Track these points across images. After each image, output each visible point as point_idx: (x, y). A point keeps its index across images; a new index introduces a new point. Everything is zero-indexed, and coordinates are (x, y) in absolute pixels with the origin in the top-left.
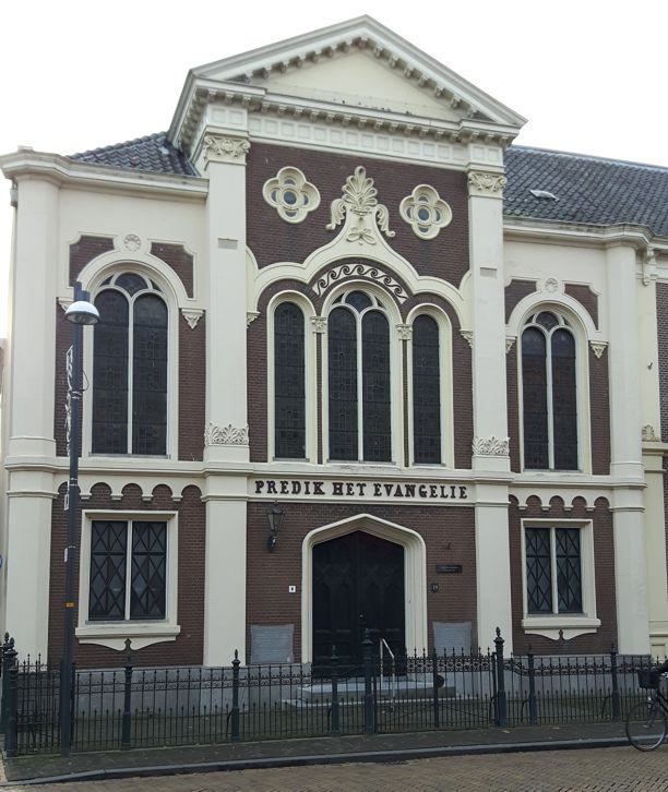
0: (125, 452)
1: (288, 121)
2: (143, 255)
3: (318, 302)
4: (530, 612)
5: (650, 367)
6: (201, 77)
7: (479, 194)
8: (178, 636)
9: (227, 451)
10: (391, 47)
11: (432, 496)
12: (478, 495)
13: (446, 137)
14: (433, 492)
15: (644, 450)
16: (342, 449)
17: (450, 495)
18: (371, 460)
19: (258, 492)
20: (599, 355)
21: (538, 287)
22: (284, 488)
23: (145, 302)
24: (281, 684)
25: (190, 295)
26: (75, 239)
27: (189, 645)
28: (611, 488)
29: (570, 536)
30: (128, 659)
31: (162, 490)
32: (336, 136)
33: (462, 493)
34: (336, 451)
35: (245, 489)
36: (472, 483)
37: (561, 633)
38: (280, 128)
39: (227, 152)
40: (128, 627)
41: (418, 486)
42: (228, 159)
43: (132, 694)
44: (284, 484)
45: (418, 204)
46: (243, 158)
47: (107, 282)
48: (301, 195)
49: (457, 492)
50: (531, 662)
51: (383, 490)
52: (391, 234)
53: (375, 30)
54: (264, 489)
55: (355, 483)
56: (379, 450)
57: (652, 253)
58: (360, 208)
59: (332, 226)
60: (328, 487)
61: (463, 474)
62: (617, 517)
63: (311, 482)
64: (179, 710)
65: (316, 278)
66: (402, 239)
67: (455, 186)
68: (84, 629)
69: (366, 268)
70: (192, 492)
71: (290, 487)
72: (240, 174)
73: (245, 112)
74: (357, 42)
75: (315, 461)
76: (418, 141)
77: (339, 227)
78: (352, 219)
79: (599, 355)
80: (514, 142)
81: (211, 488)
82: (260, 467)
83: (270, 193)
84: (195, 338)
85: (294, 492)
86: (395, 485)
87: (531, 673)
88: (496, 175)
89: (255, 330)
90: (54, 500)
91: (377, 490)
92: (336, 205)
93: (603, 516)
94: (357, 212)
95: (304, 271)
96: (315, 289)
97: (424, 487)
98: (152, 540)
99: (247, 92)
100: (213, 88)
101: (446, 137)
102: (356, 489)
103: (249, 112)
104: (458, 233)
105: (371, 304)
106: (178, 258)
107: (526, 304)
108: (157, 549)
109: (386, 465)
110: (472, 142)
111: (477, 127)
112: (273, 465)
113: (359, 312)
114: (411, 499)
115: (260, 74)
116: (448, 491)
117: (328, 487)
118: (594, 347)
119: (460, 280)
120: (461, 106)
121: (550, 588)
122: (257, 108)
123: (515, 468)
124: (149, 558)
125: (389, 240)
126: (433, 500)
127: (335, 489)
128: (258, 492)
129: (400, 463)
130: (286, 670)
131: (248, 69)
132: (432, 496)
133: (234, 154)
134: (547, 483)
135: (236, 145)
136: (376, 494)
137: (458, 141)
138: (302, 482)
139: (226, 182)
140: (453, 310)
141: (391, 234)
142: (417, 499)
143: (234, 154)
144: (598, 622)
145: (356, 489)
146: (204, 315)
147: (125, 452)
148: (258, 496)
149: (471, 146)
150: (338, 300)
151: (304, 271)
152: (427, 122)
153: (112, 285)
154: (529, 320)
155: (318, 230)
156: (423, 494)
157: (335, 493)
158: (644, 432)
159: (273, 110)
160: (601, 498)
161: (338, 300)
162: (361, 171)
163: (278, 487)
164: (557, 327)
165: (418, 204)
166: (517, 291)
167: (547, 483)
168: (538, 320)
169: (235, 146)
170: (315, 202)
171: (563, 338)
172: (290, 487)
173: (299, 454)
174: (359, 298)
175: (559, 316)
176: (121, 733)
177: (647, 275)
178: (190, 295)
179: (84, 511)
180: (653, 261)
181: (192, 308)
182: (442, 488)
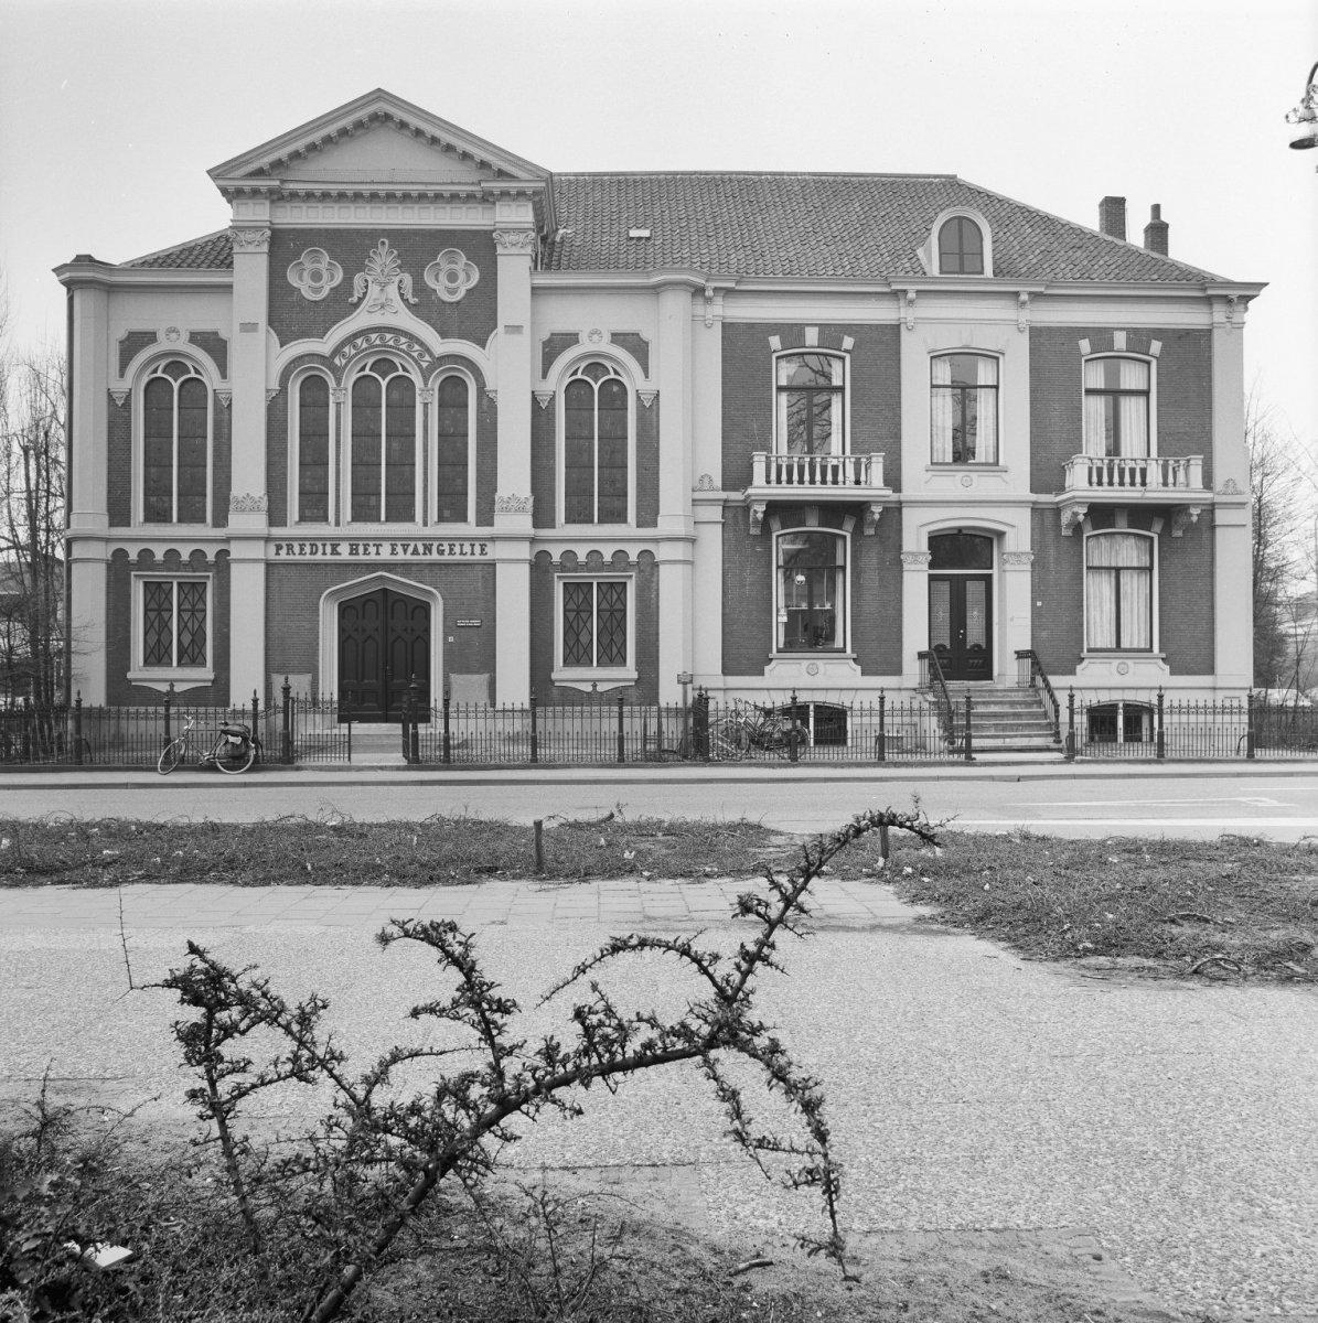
0: (592, 522)
1: (472, 206)
2: (182, 344)
4: (566, 663)
7: (243, 250)
8: (213, 682)
9: (248, 521)
12: (495, 552)
13: (470, 197)
14: (451, 550)
17: (470, 552)
18: (626, 517)
19: (277, 554)
20: (120, 403)
22: (302, 549)
23: (574, 391)
25: (224, 376)
27: (219, 690)
28: (656, 540)
29: (194, 590)
30: (169, 699)
32: (361, 213)
33: (483, 550)
36: (493, 539)
37: (595, 686)
38: (289, 212)
40: (174, 672)
41: (436, 544)
42: (251, 248)
49: (477, 549)
51: (399, 549)
52: (413, 300)
54: (284, 551)
56: (401, 509)
58: (382, 279)
60: (344, 549)
61: (485, 531)
62: (234, 567)
65: (337, 351)
66: (424, 304)
67: (482, 247)
68: (138, 671)
71: (307, 549)
73: (267, 203)
74: (374, 117)
75: (341, 524)
76: (302, 204)
77: (361, 300)
78: (374, 290)
82: (277, 531)
84: (224, 411)
85: (311, 553)
86: (412, 544)
88: (523, 231)
90: (108, 564)
91: (393, 549)
92: (358, 280)
93: (648, 566)
95: (324, 346)
96: (337, 361)
98: (196, 599)
99: (263, 184)
101: (470, 197)
102: (372, 550)
103: (272, 202)
104: (486, 293)
106: (637, 346)
108: (618, 606)
111: (498, 186)
112: (294, 529)
114: (428, 557)
115: (278, 164)
116: (467, 548)
117: (344, 549)
118: (114, 396)
119: (285, 344)
120: (483, 165)
121: (179, 635)
122: (277, 197)
125: (414, 309)
126: (451, 557)
127: (352, 549)
128: (277, 554)
131: (265, 162)
132: (450, 553)
133: (520, 245)
134: (577, 539)
135: (523, 236)
138: (319, 544)
139: (251, 273)
141: (413, 300)
143: (520, 245)
145: (372, 550)
146: (554, 396)
147: (592, 522)
148: (277, 557)
151: (324, 346)
153: (579, 376)
155: (341, 303)
159: (294, 195)
160: (143, 550)
163: (297, 549)
166: (553, 347)
167: (577, 539)
169: (257, 236)
171: (615, 389)
172: (307, 549)
174: (383, 366)
178: (224, 376)
179: (133, 573)
182: (462, 545)
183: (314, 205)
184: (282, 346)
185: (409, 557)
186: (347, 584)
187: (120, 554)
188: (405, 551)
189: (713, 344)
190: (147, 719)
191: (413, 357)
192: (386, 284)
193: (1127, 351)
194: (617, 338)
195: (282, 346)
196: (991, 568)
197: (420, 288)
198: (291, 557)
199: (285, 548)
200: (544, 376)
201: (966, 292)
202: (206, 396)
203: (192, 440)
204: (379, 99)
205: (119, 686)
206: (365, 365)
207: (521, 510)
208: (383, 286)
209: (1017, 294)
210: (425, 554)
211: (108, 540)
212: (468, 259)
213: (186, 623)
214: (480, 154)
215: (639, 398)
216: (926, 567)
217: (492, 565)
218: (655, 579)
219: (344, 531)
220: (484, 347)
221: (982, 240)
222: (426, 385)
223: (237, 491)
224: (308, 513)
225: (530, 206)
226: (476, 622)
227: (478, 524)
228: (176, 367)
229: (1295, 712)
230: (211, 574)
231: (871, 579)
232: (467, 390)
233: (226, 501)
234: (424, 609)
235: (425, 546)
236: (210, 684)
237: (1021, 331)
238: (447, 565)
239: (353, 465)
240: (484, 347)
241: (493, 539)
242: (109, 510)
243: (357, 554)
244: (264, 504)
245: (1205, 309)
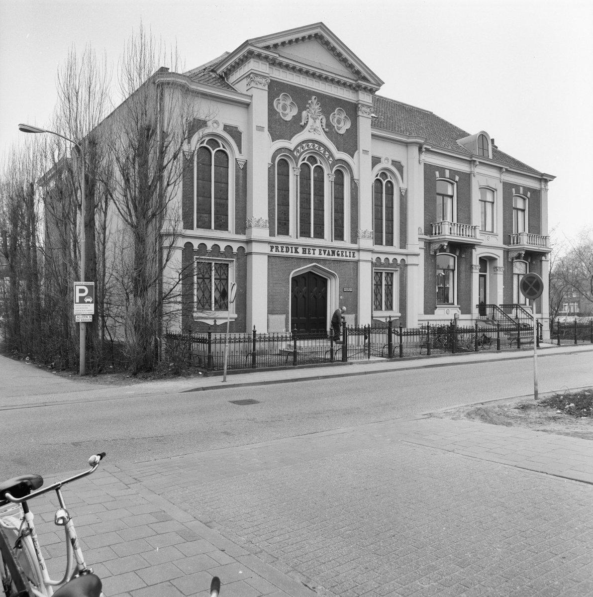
2: (220, 131)
6: (252, 45)
9: (260, 232)
13: (350, 86)
14: (342, 254)
16: (305, 233)
17: (345, 255)
18: (227, 226)
19: (271, 251)
20: (242, 167)
22: (282, 249)
24: (235, 343)
25: (240, 152)
27: (242, 323)
28: (407, 255)
29: (223, 268)
33: (354, 255)
34: (302, 232)
35: (266, 249)
36: (359, 250)
37: (215, 321)
42: (260, 86)
43: (212, 345)
44: (282, 248)
45: (282, 102)
46: (267, 87)
48: (289, 107)
50: (401, 331)
51: (322, 252)
52: (327, 130)
53: (324, 31)
54: (274, 250)
55: (311, 248)
58: (314, 116)
59: (302, 123)
60: (300, 250)
63: (294, 247)
64: (221, 353)
65: (295, 148)
66: (330, 132)
67: (352, 110)
69: (316, 145)
71: (285, 249)
75: (293, 237)
76: (259, 61)
77: (306, 124)
78: (311, 121)
80: (377, 93)
83: (278, 107)
84: (243, 172)
87: (401, 335)
89: (271, 170)
91: (320, 252)
92: (304, 113)
93: (404, 265)
95: (292, 144)
96: (295, 153)
100: (257, 51)
101: (350, 86)
102: (312, 252)
103: (269, 64)
104: (353, 132)
105: (219, 147)
106: (400, 167)
107: (378, 167)
110: (253, 58)
113: (312, 165)
114: (333, 257)
116: (348, 254)
117: (300, 250)
118: (185, 153)
120: (358, 73)
122: (274, 63)
123: (272, 234)
124: (204, 280)
125: (326, 132)
128: (271, 251)
129: (231, 233)
130: (284, 336)
131: (271, 43)
135: (369, 109)
138: (279, 246)
141: (327, 130)
142: (336, 257)
143: (263, 85)
144: (400, 315)
145: (312, 252)
149: (360, 92)
150: (304, 160)
151: (292, 144)
153: (205, 145)
154: (377, 176)
155: (297, 125)
156: (338, 255)
159: (280, 65)
162: (315, 98)
163: (280, 249)
164: (387, 180)
165: (282, 102)
168: (380, 176)
169: (263, 81)
170: (295, 112)
171: (389, 185)
173: (287, 233)
176: (256, 359)
178: (240, 152)
182: (346, 252)
183: (257, 61)
185: (326, 256)
186: (324, 268)
187: (189, 245)
190: (220, 342)
193: (440, 177)
194: (226, 128)
196: (486, 272)
197: (329, 125)
198: (277, 253)
201: (516, 172)
203: (220, 184)
205: (189, 325)
208: (315, 119)
209: (501, 168)
211: (372, 252)
214: (358, 67)
216: (478, 271)
217: (357, 262)
218: (405, 272)
219: (295, 241)
220: (273, 141)
221: (488, 145)
226: (350, 290)
229: (365, 331)
230: (234, 259)
231: (463, 275)
232: (343, 177)
236: (234, 320)
238: (340, 261)
240: (273, 141)
241: (359, 250)
245: (468, 165)
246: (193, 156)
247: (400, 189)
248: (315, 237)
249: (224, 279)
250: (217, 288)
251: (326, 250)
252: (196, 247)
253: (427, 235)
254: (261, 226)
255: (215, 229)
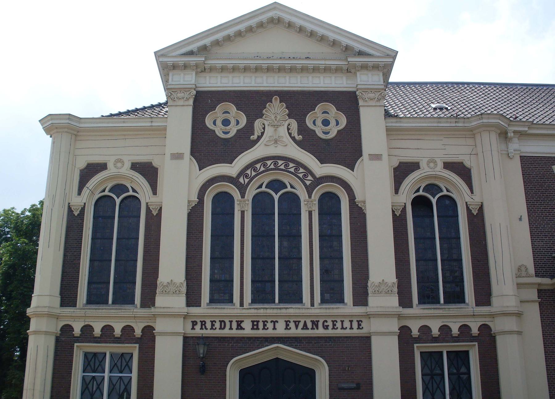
2: (440, 170)
3: (243, 189)
5: (520, 219)
7: (366, 104)
10: (294, 19)
11: (333, 328)
12: (369, 327)
14: (334, 325)
15: (518, 284)
17: (349, 327)
19: (193, 328)
20: (76, 213)
21: (130, 166)
22: (213, 325)
25: (155, 193)
26: (155, 164)
31: (464, 329)
33: (359, 325)
36: (368, 316)
39: (371, 99)
42: (181, 102)
47: (418, 190)
51: (292, 325)
54: (198, 327)
57: (512, 134)
59: (254, 137)
60: (247, 325)
61: (360, 310)
62: (158, 340)
65: (242, 173)
70: (484, 328)
72: (188, 112)
77: (259, 138)
78: (269, 131)
79: (76, 213)
81: (160, 326)
82: (194, 310)
91: (287, 325)
92: (258, 124)
94: (273, 126)
96: (241, 180)
97: (326, 321)
102: (270, 325)
109: (462, 305)
114: (315, 331)
117: (247, 325)
119: (203, 168)
122: (202, 70)
124: (432, 378)
125: (299, 143)
127: (253, 325)
128: (193, 328)
132: (333, 328)
136: (286, 328)
137: (348, 71)
140: (349, 186)
141: (299, 138)
145: (270, 325)
147: (106, 302)
148: (193, 331)
149: (358, 73)
150: (260, 186)
152: (323, 62)
156: (326, 327)
157: (253, 329)
158: (519, 269)
161: (260, 186)
169: (186, 95)
171: (447, 202)
175: (442, 186)
177: (511, 150)
178: (155, 193)
180: (516, 140)
181: (474, 200)
182: (342, 322)
184: (200, 170)
187: (67, 329)
188: (297, 327)
189: (516, 167)
191: (299, 177)
192: (278, 126)
194: (448, 166)
195: (200, 170)
199: (199, 324)
200: (397, 191)
202: (139, 209)
204: (274, 9)
206: (262, 184)
207: (177, 292)
210: (312, 328)
212: (337, 110)
213: (438, 387)
215: (468, 208)
222: (310, 197)
223: (163, 277)
224: (216, 297)
225: (381, 74)
227: (478, 304)
228: (276, 185)
233: (154, 286)
234: (310, 375)
235: (313, 322)
237: (511, 158)
239: (252, 258)
241: (368, 316)
242: (61, 293)
243: (258, 329)
244: (184, 289)
246: (404, 209)
247: (467, 205)
248: (447, 302)
249: (437, 375)
250: (427, 388)
251: (299, 322)
252: (415, 332)
253: (543, 276)
254: (171, 293)
255: (446, 302)
